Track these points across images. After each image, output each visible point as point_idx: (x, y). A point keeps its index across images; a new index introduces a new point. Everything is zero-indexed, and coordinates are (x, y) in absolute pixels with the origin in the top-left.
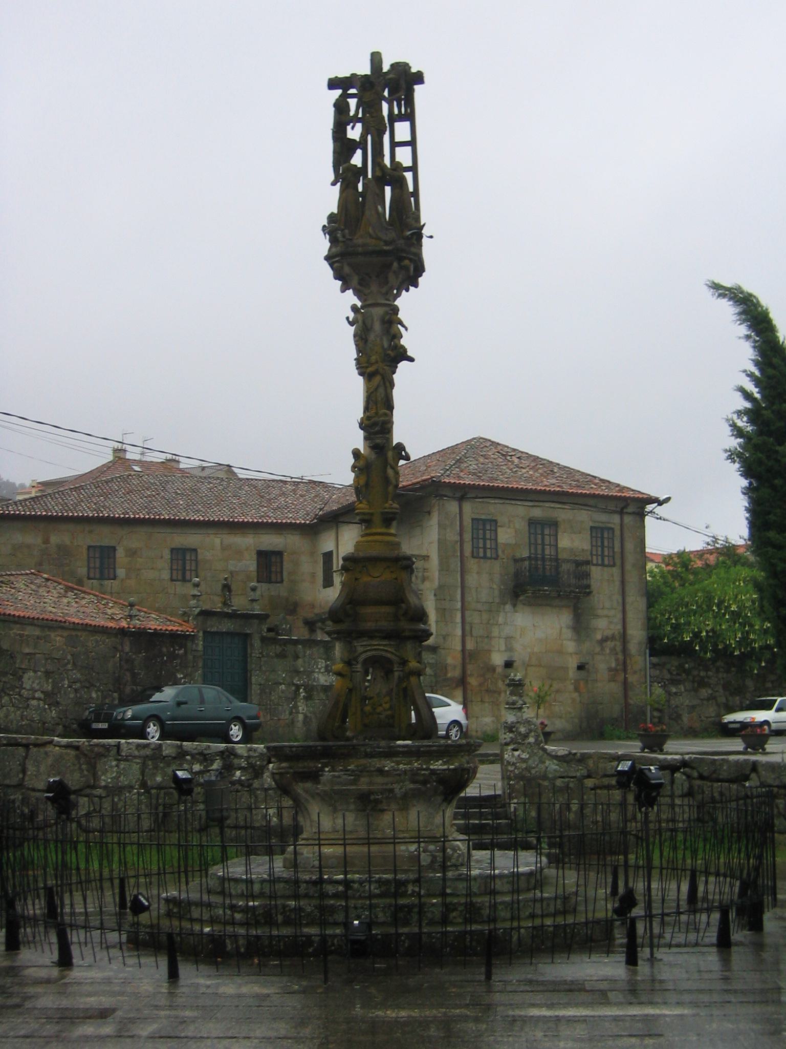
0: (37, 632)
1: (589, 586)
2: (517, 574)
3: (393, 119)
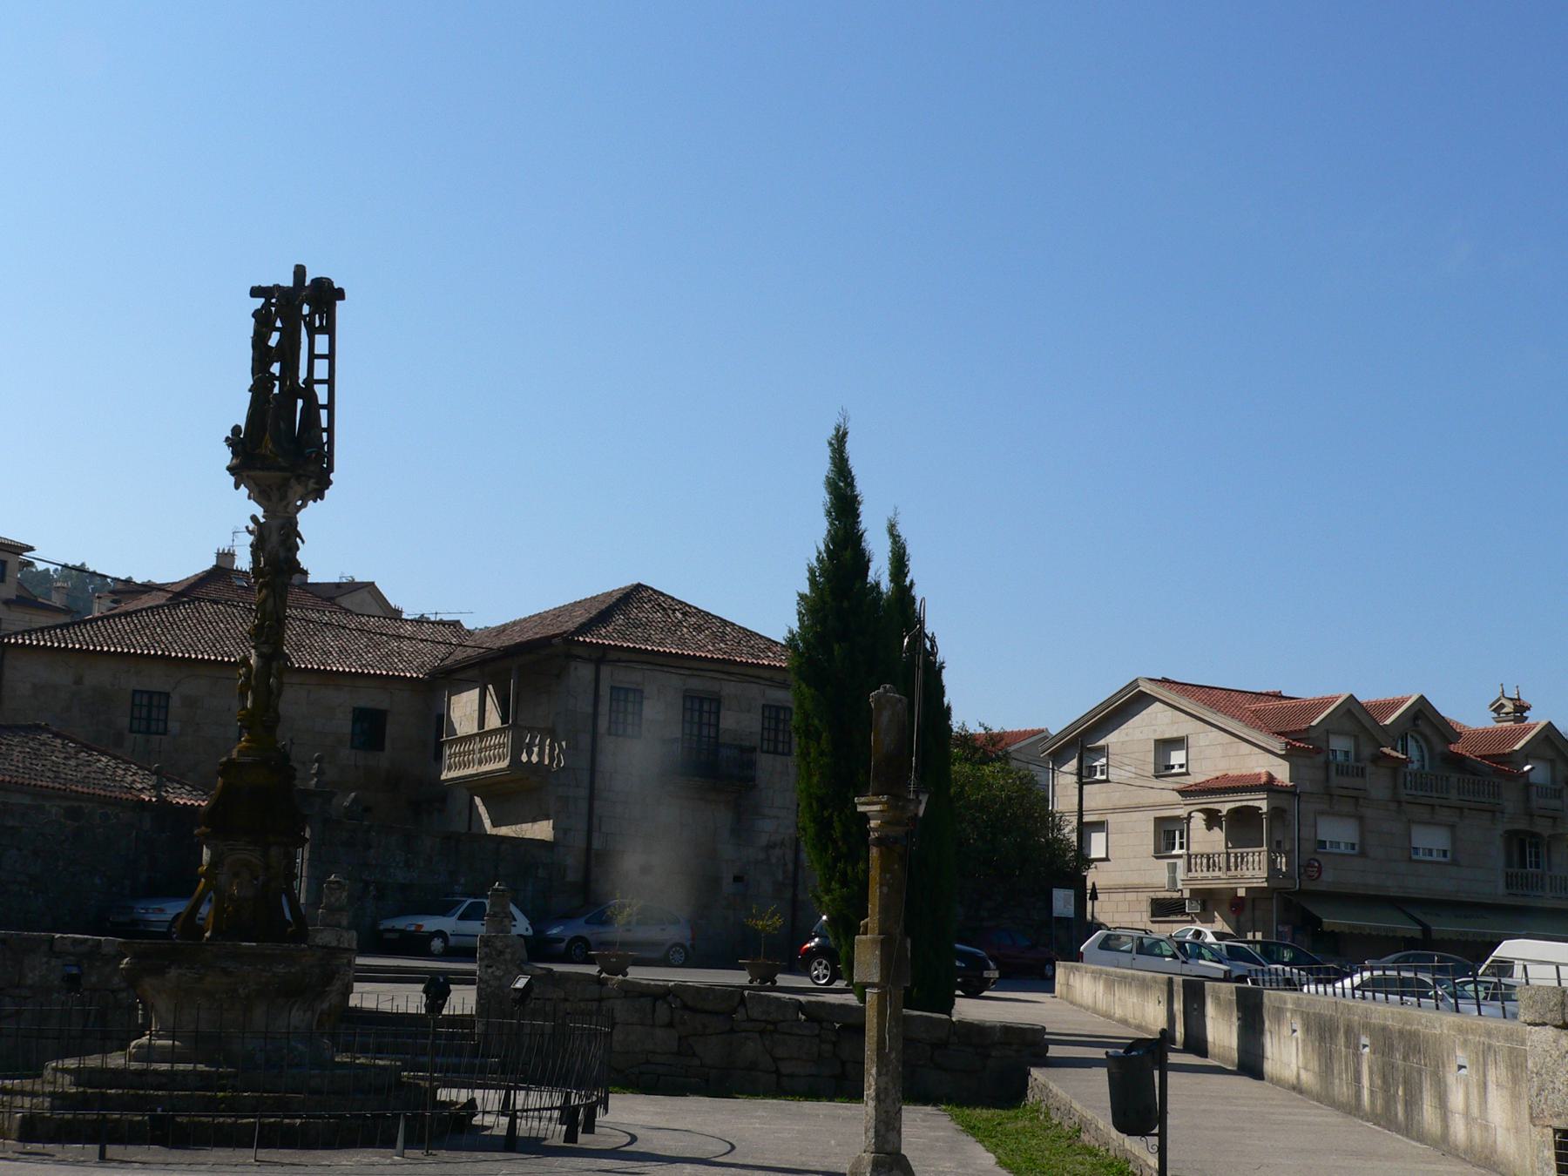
1: (753, 779)
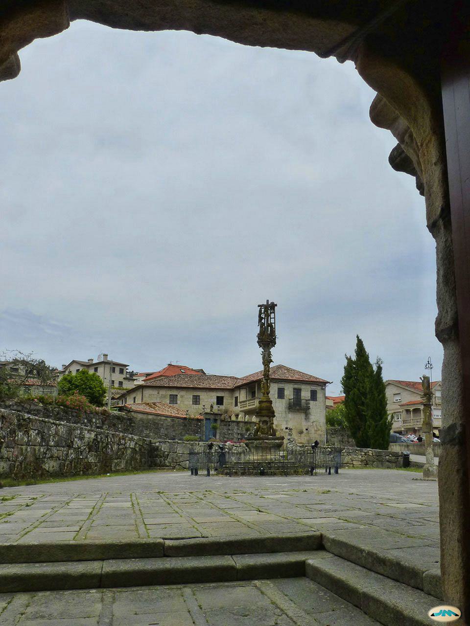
0: (165, 418)
2: (290, 403)
3: (271, 313)
